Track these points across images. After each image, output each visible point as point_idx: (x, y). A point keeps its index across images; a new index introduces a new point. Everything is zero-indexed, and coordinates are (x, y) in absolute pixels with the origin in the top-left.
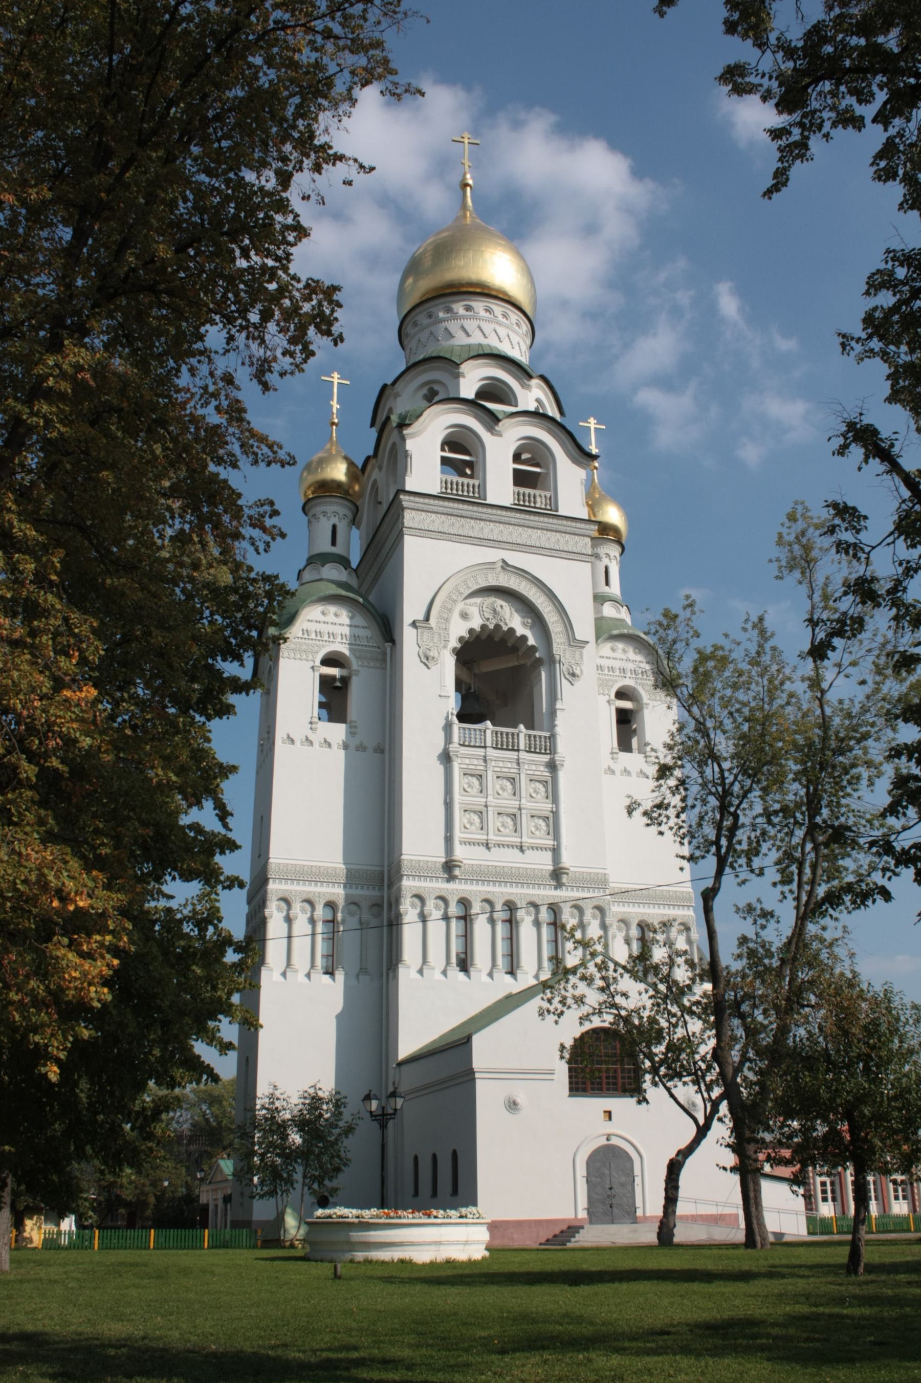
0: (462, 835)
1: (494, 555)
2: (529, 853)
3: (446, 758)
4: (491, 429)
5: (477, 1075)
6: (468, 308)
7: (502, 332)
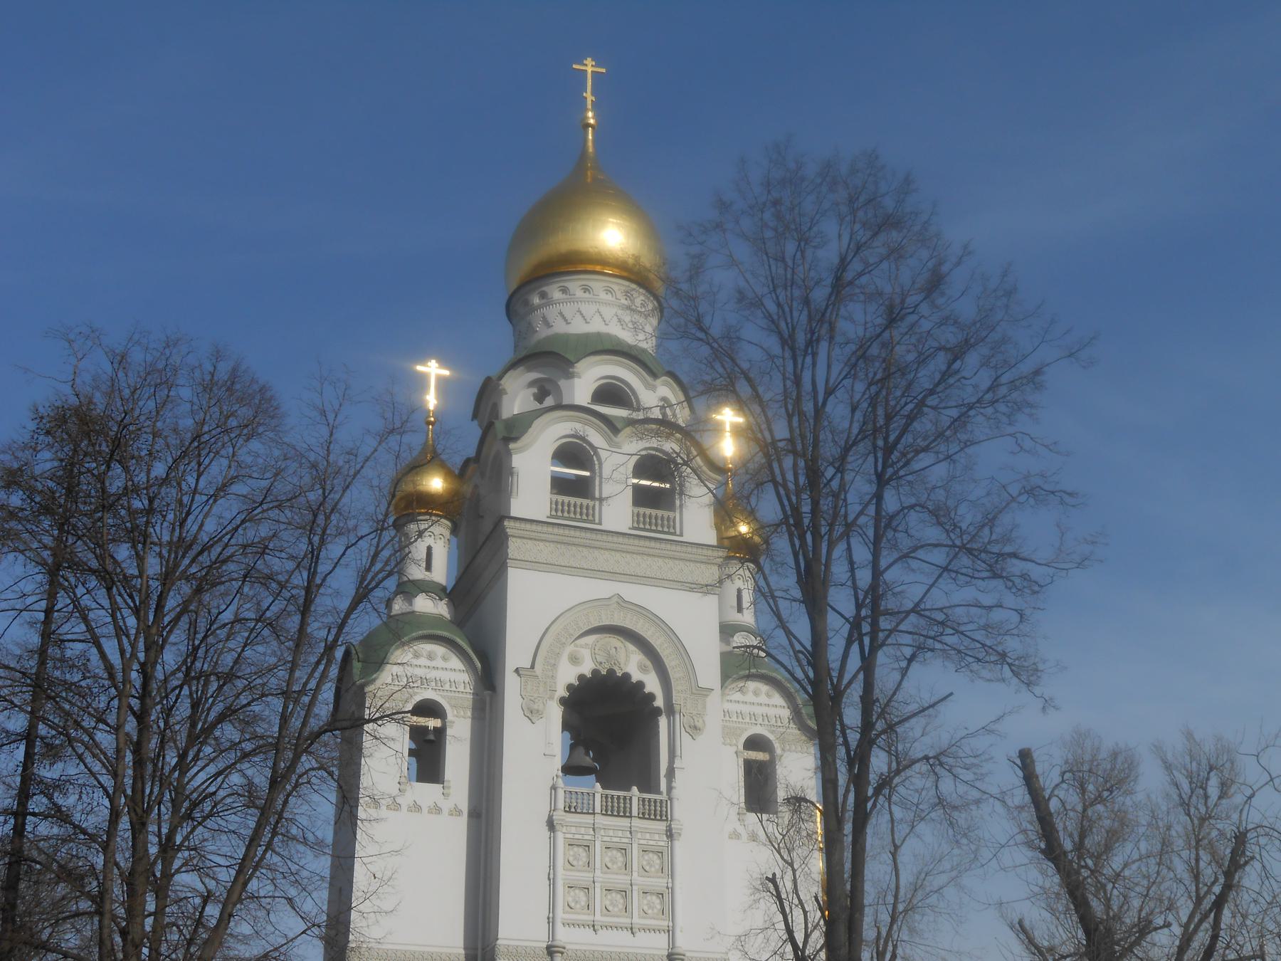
0: (567, 916)
1: (604, 589)
3: (551, 825)
6: (564, 290)
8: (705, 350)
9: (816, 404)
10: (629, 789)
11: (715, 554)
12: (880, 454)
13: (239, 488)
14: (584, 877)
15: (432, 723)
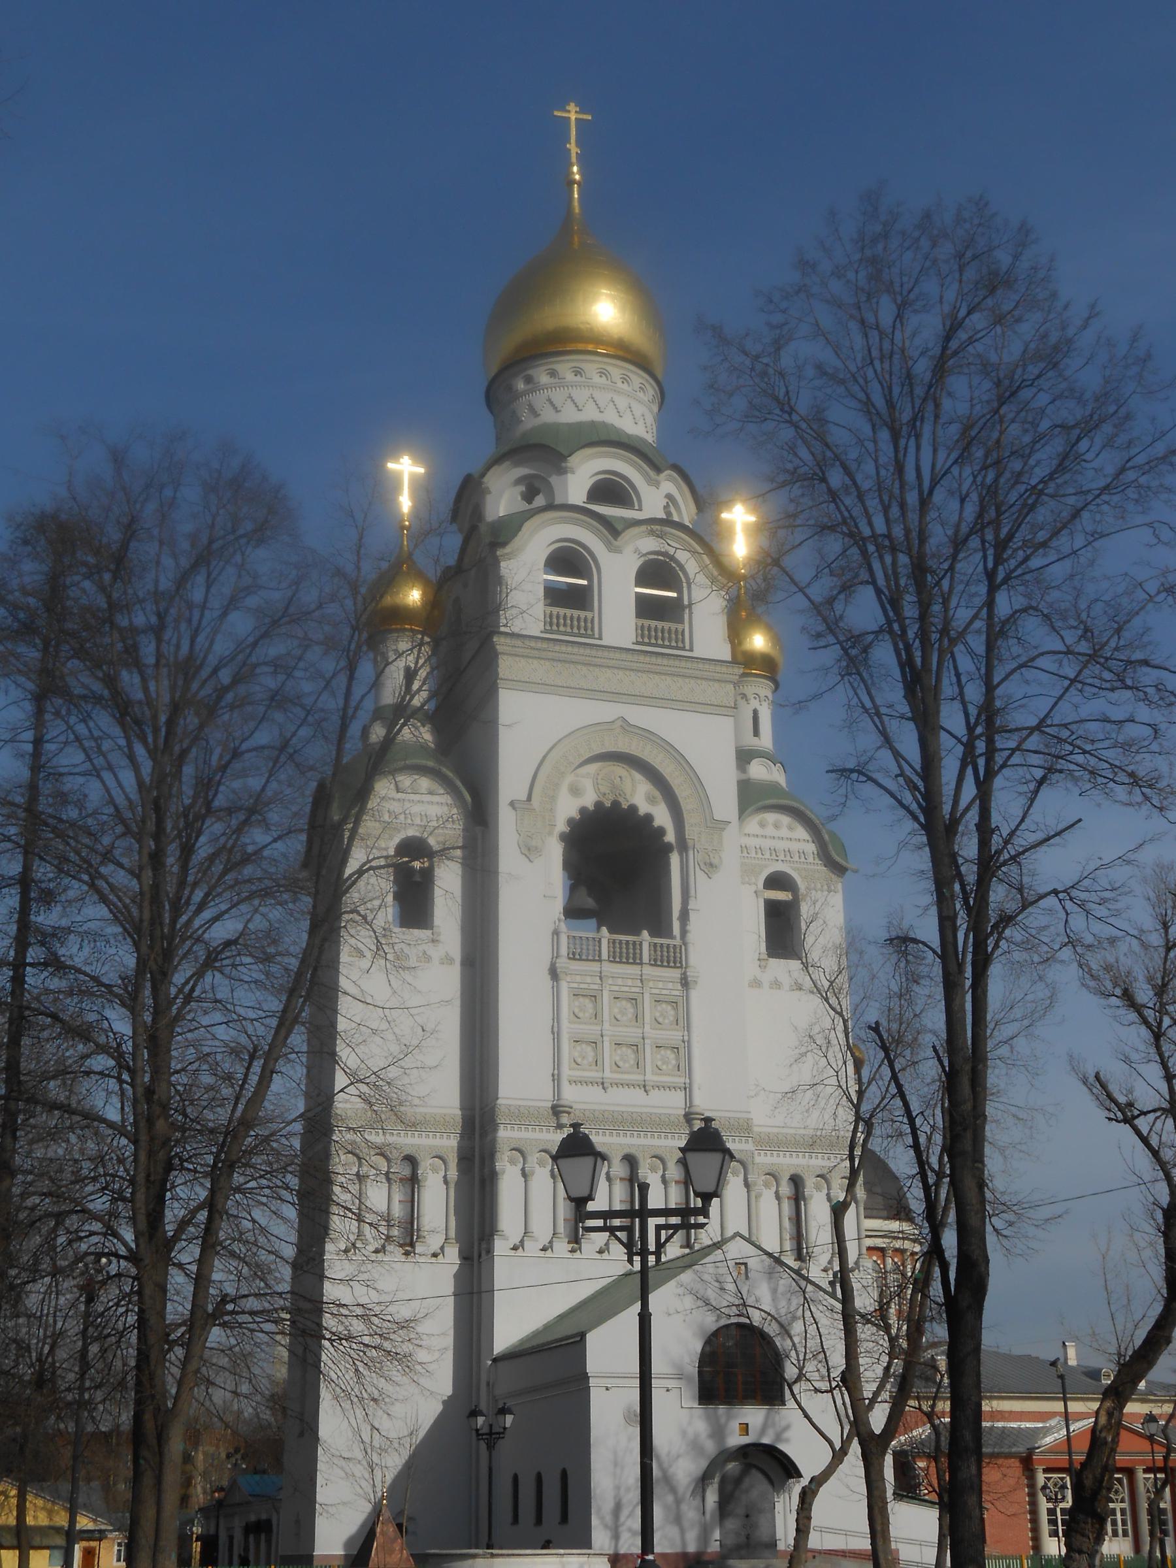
0: (571, 1073)
1: (607, 711)
2: (654, 1093)
3: (554, 974)
4: (611, 548)
5: (592, 1382)
6: (553, 374)
7: (622, 402)
8: (787, 433)
9: (921, 493)
10: (638, 933)
11: (730, 670)
12: (990, 552)
13: (252, 601)
14: (590, 1030)
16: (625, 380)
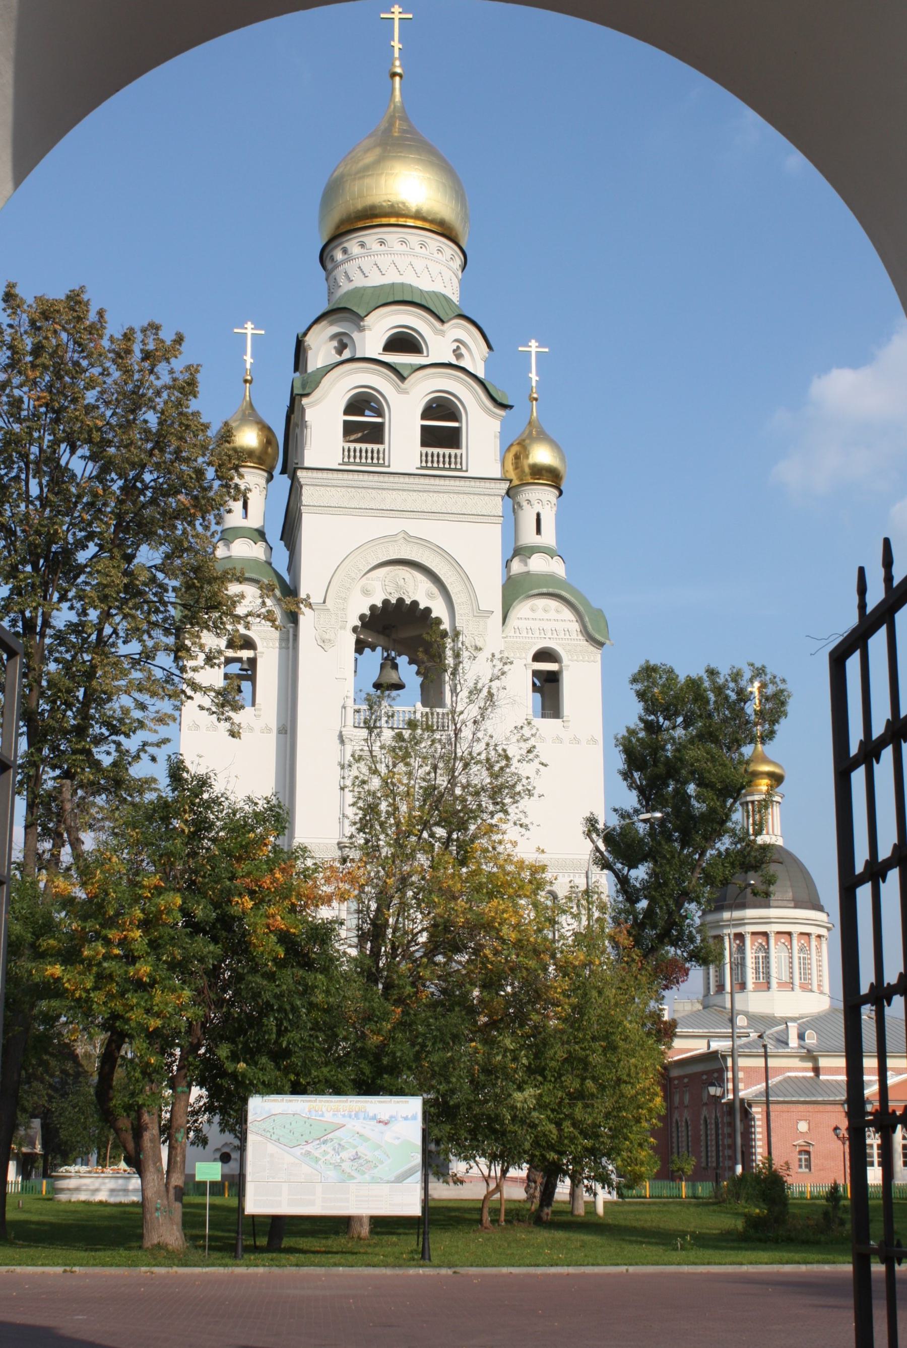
6: (362, 245)
7: (419, 264)
15: (245, 654)
16: (423, 245)
